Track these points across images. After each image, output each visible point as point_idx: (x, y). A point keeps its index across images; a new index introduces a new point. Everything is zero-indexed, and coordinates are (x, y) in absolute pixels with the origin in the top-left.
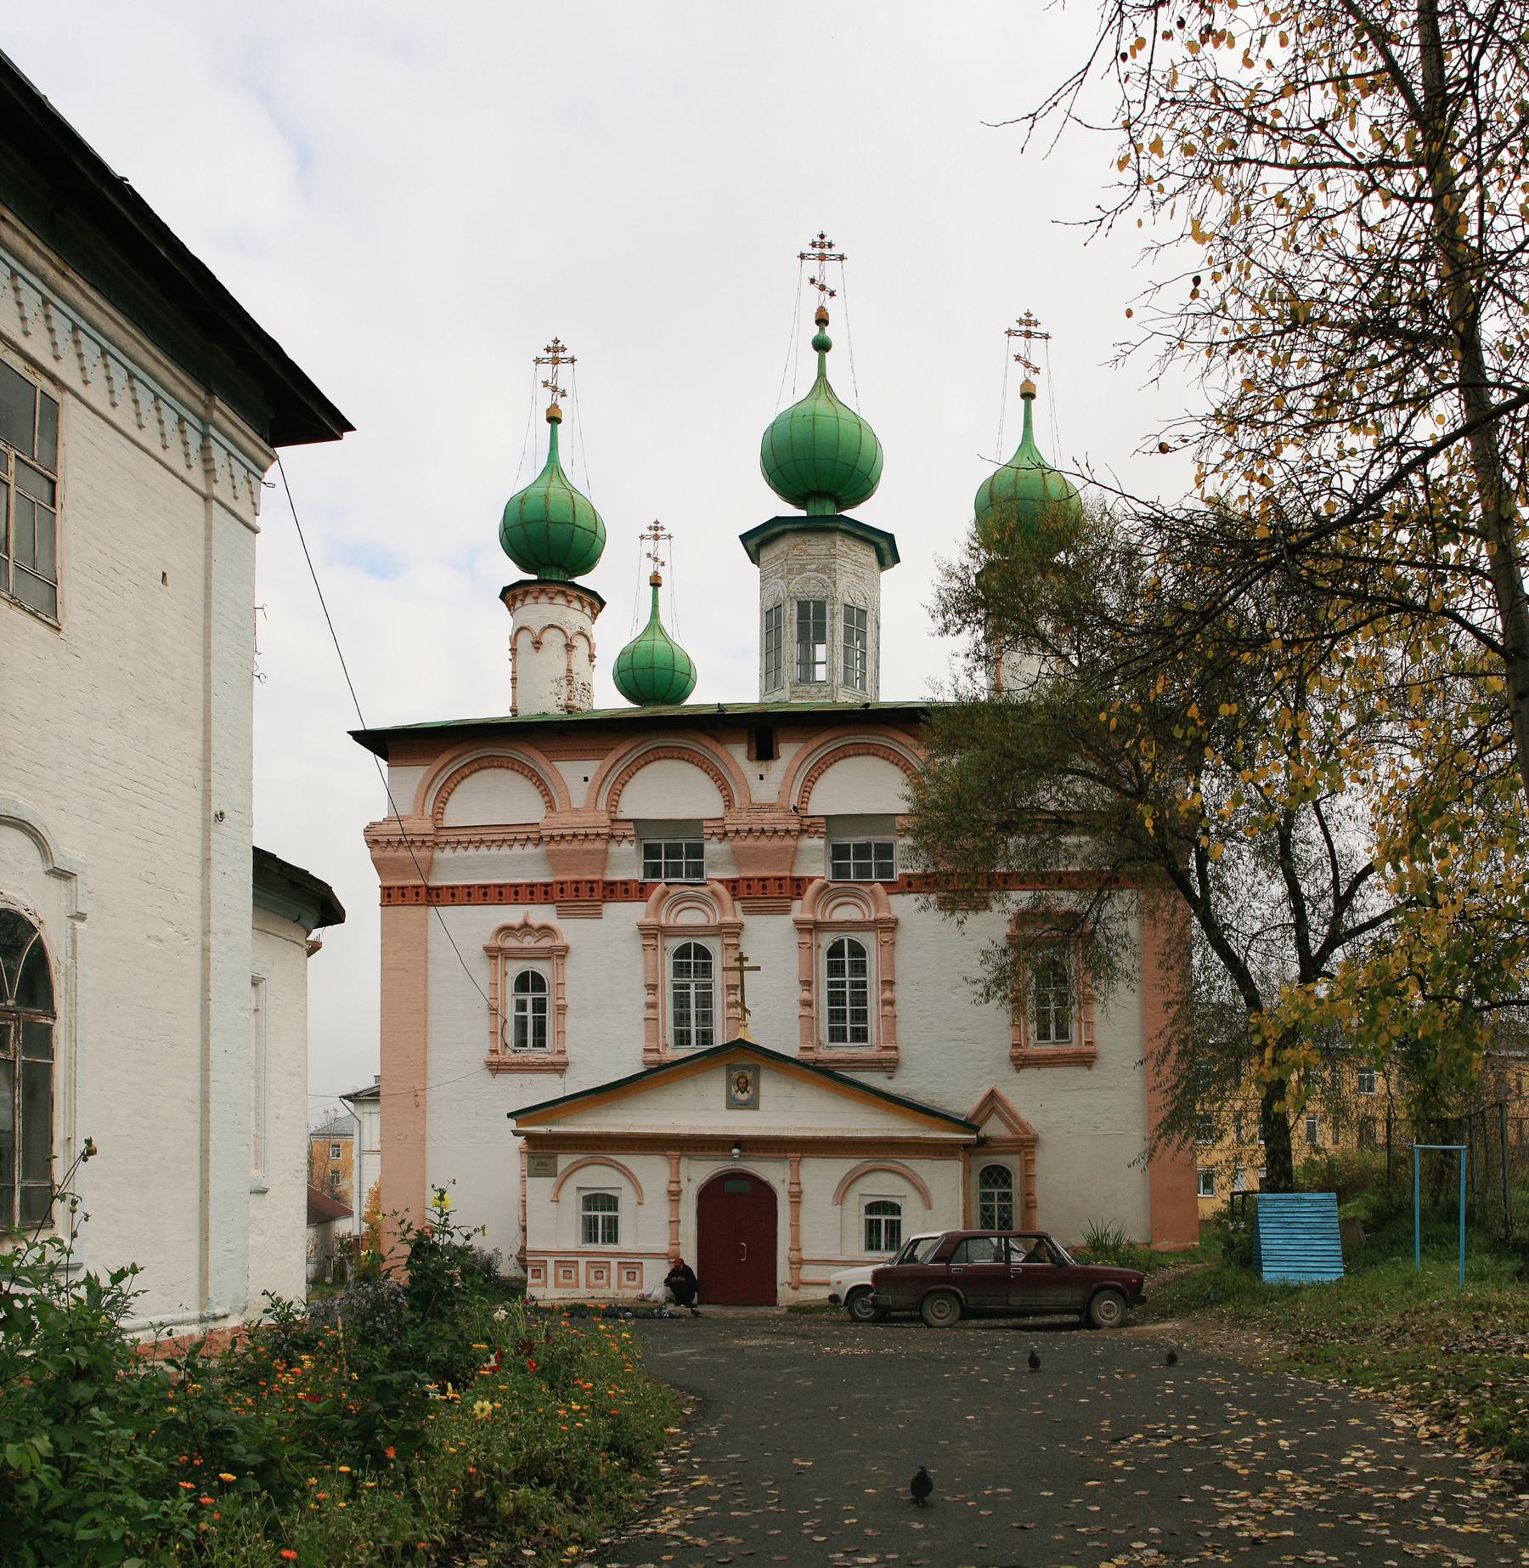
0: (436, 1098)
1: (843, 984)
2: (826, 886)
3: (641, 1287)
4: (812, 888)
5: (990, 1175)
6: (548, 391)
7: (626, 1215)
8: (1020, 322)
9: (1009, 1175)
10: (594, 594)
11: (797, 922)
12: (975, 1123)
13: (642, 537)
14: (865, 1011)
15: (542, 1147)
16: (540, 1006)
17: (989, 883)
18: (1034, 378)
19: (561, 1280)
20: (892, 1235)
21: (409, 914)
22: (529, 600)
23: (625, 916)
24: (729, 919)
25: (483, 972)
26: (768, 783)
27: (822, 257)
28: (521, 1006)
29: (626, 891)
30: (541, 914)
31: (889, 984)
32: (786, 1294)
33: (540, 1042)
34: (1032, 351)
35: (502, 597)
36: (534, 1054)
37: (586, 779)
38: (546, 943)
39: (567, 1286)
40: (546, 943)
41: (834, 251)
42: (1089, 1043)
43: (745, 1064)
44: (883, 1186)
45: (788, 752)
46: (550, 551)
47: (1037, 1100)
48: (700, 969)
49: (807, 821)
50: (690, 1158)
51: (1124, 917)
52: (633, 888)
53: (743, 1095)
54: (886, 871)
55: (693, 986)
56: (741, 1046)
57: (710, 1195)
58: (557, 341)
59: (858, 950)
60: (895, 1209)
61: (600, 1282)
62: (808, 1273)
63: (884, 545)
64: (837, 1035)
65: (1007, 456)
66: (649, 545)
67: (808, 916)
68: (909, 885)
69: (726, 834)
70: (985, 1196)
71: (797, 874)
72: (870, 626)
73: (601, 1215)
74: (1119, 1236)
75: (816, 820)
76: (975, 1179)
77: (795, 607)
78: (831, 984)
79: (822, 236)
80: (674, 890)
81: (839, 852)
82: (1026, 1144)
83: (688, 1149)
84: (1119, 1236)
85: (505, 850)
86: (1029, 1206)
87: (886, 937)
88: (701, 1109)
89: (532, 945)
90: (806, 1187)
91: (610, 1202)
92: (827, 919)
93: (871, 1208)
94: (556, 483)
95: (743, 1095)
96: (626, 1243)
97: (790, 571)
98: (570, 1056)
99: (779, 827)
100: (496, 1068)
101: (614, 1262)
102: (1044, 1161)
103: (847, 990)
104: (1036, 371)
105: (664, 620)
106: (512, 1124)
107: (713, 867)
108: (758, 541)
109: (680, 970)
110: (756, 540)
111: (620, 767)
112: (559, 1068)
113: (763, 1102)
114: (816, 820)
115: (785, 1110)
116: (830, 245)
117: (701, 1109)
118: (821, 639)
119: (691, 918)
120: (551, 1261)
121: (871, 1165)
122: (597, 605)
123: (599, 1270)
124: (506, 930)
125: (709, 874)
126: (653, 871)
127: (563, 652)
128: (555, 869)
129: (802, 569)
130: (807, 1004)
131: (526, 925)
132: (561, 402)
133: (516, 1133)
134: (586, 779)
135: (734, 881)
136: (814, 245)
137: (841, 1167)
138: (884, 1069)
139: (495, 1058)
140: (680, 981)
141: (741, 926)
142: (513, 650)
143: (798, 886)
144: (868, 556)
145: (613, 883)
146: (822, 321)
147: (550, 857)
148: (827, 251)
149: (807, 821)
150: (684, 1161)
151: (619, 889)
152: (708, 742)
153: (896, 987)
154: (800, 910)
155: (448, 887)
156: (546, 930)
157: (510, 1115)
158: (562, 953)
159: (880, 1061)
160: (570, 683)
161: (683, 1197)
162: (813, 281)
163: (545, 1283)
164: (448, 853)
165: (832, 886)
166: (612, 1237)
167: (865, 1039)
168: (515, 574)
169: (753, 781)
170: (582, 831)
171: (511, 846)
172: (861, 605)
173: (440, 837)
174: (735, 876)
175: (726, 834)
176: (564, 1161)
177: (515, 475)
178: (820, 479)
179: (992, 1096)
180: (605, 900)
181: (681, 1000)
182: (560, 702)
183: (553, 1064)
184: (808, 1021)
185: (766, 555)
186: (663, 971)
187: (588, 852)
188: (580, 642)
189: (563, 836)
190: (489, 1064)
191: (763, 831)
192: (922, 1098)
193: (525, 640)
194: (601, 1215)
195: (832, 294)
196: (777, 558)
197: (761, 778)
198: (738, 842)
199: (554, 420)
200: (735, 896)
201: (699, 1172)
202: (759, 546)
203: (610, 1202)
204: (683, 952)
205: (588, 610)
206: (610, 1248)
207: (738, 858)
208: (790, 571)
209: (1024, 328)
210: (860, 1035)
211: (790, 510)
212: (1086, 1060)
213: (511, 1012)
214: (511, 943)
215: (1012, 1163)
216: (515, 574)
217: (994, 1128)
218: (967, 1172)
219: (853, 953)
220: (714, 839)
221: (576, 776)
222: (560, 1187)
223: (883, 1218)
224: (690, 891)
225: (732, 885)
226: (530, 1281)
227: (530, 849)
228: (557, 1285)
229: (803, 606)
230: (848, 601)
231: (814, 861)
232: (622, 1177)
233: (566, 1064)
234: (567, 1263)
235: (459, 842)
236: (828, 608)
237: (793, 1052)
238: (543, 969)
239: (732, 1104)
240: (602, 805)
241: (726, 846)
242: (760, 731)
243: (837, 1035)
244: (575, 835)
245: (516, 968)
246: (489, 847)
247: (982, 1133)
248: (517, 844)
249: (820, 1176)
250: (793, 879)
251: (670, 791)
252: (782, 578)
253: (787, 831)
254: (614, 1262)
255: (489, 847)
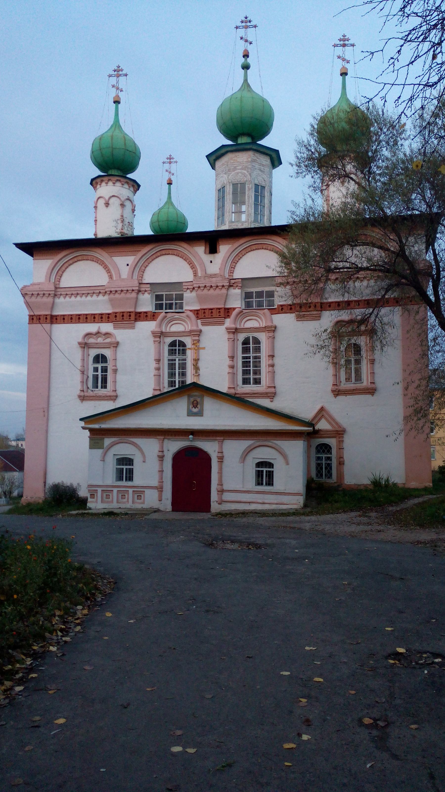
0: (54, 411)
1: (249, 358)
2: (242, 312)
3: (143, 503)
4: (234, 313)
5: (321, 448)
6: (114, 89)
7: (137, 468)
8: (340, 40)
9: (330, 448)
10: (134, 181)
11: (227, 329)
12: (313, 423)
13: (164, 163)
14: (260, 370)
15: (97, 435)
16: (105, 370)
17: (321, 307)
18: (347, 66)
19: (104, 499)
20: (269, 478)
21: (38, 327)
22: (104, 184)
23: (146, 327)
24: (195, 328)
25: (78, 354)
26: (214, 264)
27: (246, 27)
28: (96, 370)
29: (147, 316)
30: (106, 327)
31: (272, 356)
32: (215, 507)
33: (104, 386)
34: (346, 53)
35: (91, 184)
36: (100, 391)
37: (128, 265)
38: (108, 340)
39: (108, 502)
40: (108, 340)
41: (252, 23)
42: (374, 383)
43: (195, 393)
44: (264, 453)
45: (224, 248)
46: (116, 163)
47: (346, 411)
48: (181, 352)
49: (233, 281)
50: (169, 439)
51: (392, 318)
52: (149, 315)
53: (195, 409)
54: (271, 303)
55: (177, 360)
56: (195, 386)
57: (180, 459)
58: (170, 156)
59: (257, 341)
60: (271, 465)
61: (124, 500)
62: (227, 496)
63: (274, 155)
64: (246, 381)
65: (334, 102)
66: (167, 166)
67: (233, 326)
68: (282, 309)
69: (194, 288)
70: (318, 458)
71: (227, 306)
72: (267, 194)
73: (125, 469)
74: (387, 480)
75: (237, 281)
76: (313, 450)
77: (231, 187)
78: (244, 358)
79: (246, 18)
80: (169, 315)
81: (248, 295)
82: (339, 433)
83: (168, 435)
84: (387, 480)
85: (89, 298)
86: (341, 463)
87: (271, 334)
88: (175, 415)
89: (102, 341)
90: (226, 454)
91: (129, 461)
92: (242, 327)
93: (259, 465)
94: (117, 131)
95: (195, 409)
96: (138, 480)
97: (229, 170)
98: (119, 392)
99: (219, 284)
100: (83, 398)
101: (131, 490)
102: (348, 440)
103: (251, 360)
104: (348, 62)
105: (174, 200)
106: (83, 424)
107: (187, 304)
108: (214, 158)
109: (172, 352)
110: (214, 157)
111: (144, 259)
112: (114, 398)
113: (205, 412)
114: (237, 281)
115: (216, 416)
116: (250, 21)
117: (175, 415)
118: (244, 203)
119: (176, 328)
120: (99, 490)
121: (258, 444)
122: (136, 186)
123: (123, 495)
124: (88, 335)
125: (185, 307)
126: (159, 307)
127: (119, 208)
128: (113, 306)
129: (235, 169)
130: (232, 367)
131: (98, 333)
132: (121, 94)
133: (84, 428)
134: (128, 265)
135: (197, 310)
136: (242, 22)
137: (245, 444)
138: (268, 397)
139: (82, 394)
140: (171, 358)
141: (201, 331)
142: (96, 207)
143: (228, 312)
144: (266, 161)
145: (140, 313)
146: (246, 56)
147: (111, 300)
148: (248, 24)
149: (233, 281)
150: (166, 441)
151: (142, 315)
152: (185, 245)
153: (274, 358)
154: (229, 322)
155: (61, 315)
156: (107, 335)
157: (81, 420)
158: (116, 345)
159: (267, 393)
160: (123, 221)
161: (165, 458)
162: (242, 38)
163: (97, 502)
164: (62, 299)
165: (245, 311)
166: (130, 478)
167: (260, 383)
168: (98, 172)
169: (207, 263)
170: (125, 289)
171: (92, 296)
172: (263, 184)
173: (57, 292)
174: (198, 308)
175: (194, 288)
176: (107, 441)
177: (99, 125)
178: (246, 130)
179: (322, 409)
180: (136, 320)
181: (172, 366)
182: (117, 231)
183: (110, 396)
184: (233, 375)
185: (218, 164)
186: (164, 353)
187: (128, 299)
188: (128, 203)
189: (116, 291)
190: (80, 396)
191: (211, 287)
192: (287, 411)
193: (101, 202)
194: (125, 469)
195: (251, 43)
196: (223, 164)
197: (211, 262)
198: (200, 292)
199: (117, 102)
200: (198, 318)
201: (174, 446)
202: (215, 160)
203: (129, 461)
204: (173, 344)
205: (132, 189)
206: (130, 483)
207: (200, 299)
208: (229, 170)
209: (342, 42)
210: (257, 382)
211: (230, 143)
212: (371, 391)
213: (91, 373)
214: (92, 340)
215: (332, 442)
216: (98, 172)
217: (323, 425)
218: (309, 446)
219: (254, 343)
220: (188, 291)
221: (124, 262)
222: (105, 454)
223: (265, 470)
224: (177, 316)
225: (197, 313)
226: (89, 500)
227: (101, 297)
228: (102, 501)
229: (235, 185)
230: (256, 182)
231: (235, 300)
232: (137, 450)
233: (117, 396)
234: (107, 492)
235: (67, 294)
236: (247, 186)
237: (224, 390)
238: (107, 353)
239: (190, 414)
240: (135, 277)
241: (194, 294)
242: (211, 240)
243: (246, 381)
244: (122, 291)
245: (93, 352)
246: (81, 297)
247: (317, 428)
248: (95, 295)
249: (234, 448)
250: (225, 309)
251: (168, 268)
252: (225, 174)
253: (223, 286)
254: (131, 490)
255: (81, 297)
